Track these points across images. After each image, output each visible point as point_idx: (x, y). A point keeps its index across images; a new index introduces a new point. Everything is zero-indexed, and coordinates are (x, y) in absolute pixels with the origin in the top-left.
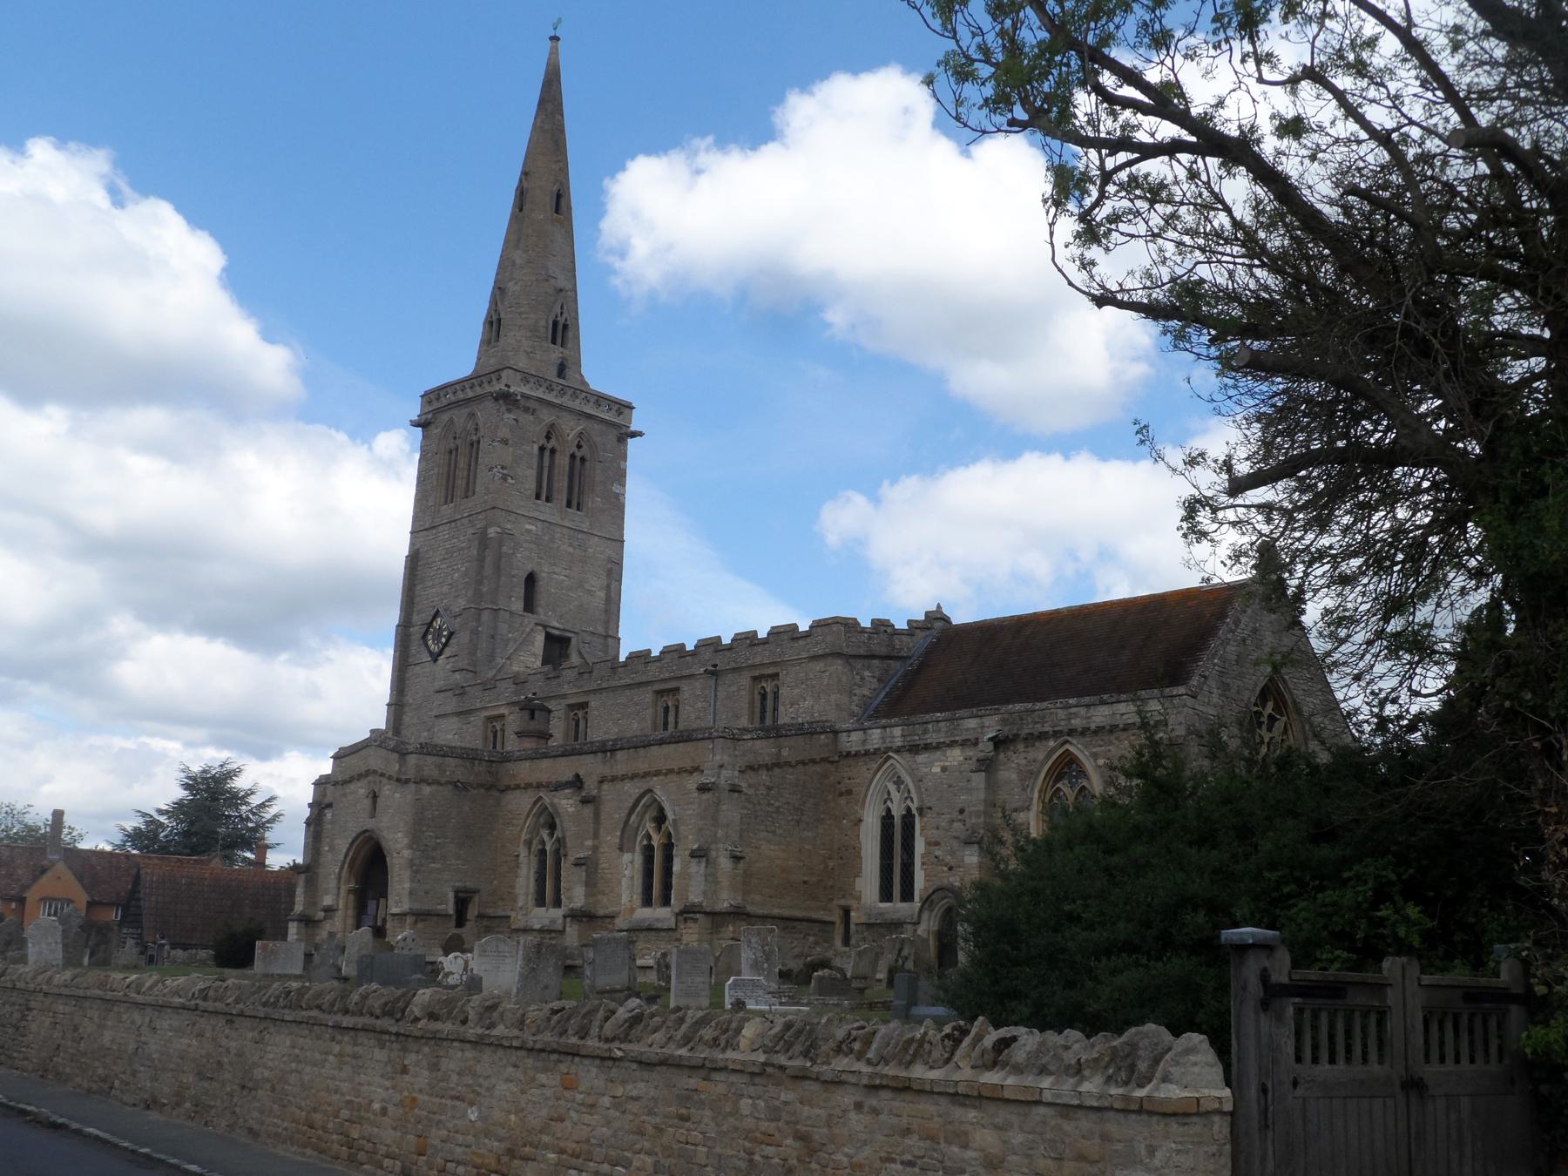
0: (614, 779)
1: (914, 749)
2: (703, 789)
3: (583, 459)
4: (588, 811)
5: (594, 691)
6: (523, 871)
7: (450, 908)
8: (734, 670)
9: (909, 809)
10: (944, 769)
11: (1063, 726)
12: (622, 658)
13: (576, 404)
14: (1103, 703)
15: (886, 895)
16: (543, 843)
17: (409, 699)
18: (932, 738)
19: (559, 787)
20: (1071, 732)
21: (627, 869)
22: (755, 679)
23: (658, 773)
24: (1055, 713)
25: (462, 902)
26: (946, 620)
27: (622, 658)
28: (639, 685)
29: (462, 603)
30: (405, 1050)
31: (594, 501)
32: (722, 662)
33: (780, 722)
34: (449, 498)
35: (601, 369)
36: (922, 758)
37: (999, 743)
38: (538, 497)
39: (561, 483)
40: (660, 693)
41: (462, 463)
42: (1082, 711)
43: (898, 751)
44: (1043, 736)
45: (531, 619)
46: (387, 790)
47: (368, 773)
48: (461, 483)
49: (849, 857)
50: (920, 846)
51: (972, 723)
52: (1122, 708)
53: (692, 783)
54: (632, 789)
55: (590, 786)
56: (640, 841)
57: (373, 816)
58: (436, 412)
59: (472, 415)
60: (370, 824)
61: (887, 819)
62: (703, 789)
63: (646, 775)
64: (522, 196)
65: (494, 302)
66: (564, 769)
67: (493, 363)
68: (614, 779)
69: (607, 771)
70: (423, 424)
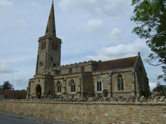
0: (68, 78)
1: (101, 74)
2: (79, 79)
3: (57, 45)
4: (65, 82)
5: (62, 69)
6: (56, 89)
7: (48, 93)
8: (79, 66)
9: (100, 81)
10: (105, 76)
11: (120, 71)
12: (61, 66)
13: (56, 39)
14: (124, 69)
15: (98, 90)
16: (58, 85)
17: (38, 71)
18: (104, 73)
19: (61, 79)
20: (121, 72)
21: (69, 88)
22: (69, 69)
23: (73, 77)
24: (119, 70)
25: (49, 92)
26: (101, 61)
27: (61, 66)
28: (67, 68)
29: (45, 60)
30: (88, 106)
31: (58, 50)
32: (77, 66)
33: (85, 71)
34: (42, 49)
35: (58, 36)
36: (102, 75)
37: (112, 73)
38: (52, 49)
39: (55, 48)
40: (69, 69)
41: (44, 45)
42: (122, 70)
43: (99, 75)
44: (117, 73)
45: (52, 62)
46: (41, 80)
47: (38, 78)
48: (44, 47)
49: (93, 86)
50: (102, 85)
51: (108, 71)
52: (127, 69)
53: (78, 78)
54: (70, 79)
55: (65, 79)
56: (71, 85)
57: (39, 82)
58: (41, 40)
59: (45, 40)
60: (39, 83)
61: (98, 82)
62: (79, 79)
63: (72, 77)
64: (50, 17)
65: (47, 28)
66: (61, 77)
67: (47, 35)
68: (68, 78)
69: (67, 77)
70: (39, 41)
